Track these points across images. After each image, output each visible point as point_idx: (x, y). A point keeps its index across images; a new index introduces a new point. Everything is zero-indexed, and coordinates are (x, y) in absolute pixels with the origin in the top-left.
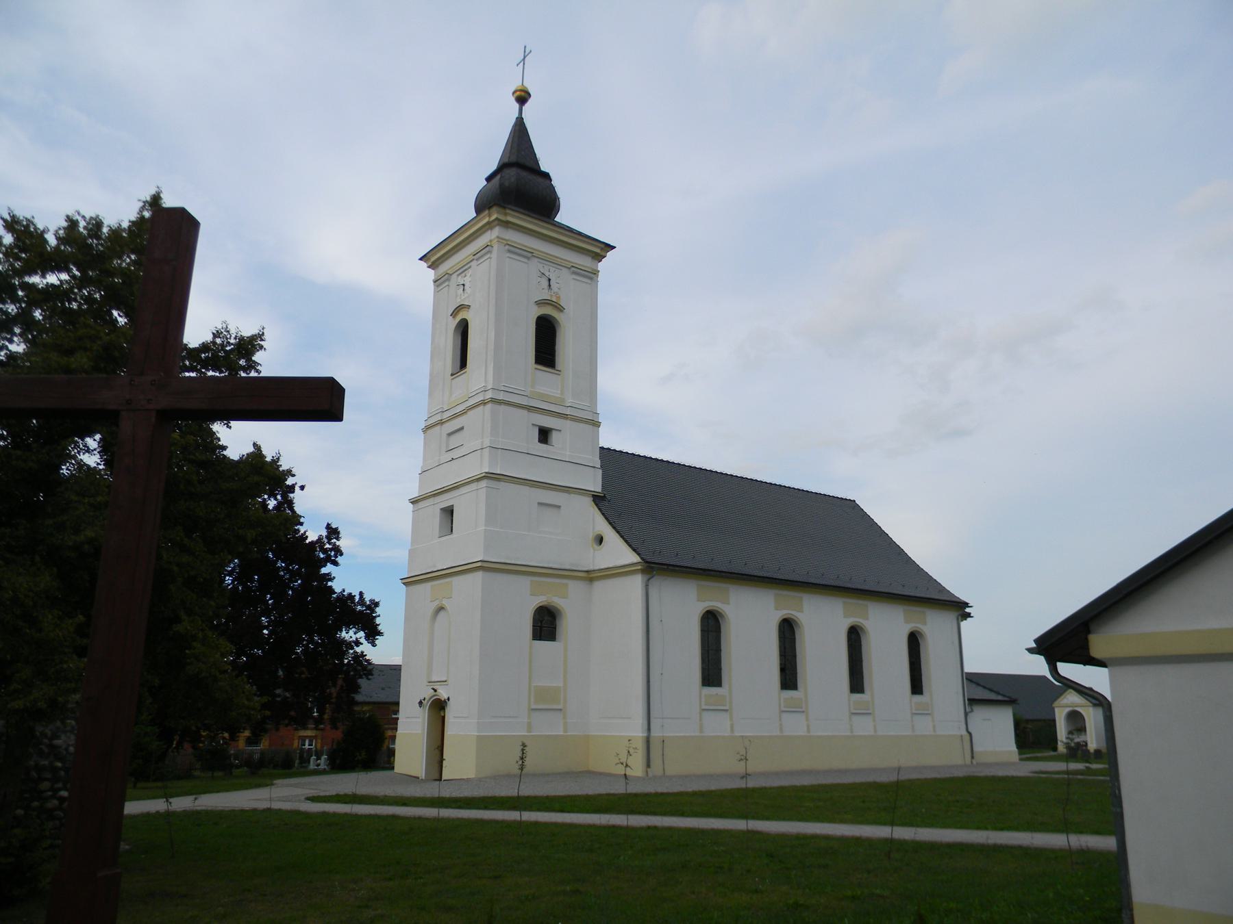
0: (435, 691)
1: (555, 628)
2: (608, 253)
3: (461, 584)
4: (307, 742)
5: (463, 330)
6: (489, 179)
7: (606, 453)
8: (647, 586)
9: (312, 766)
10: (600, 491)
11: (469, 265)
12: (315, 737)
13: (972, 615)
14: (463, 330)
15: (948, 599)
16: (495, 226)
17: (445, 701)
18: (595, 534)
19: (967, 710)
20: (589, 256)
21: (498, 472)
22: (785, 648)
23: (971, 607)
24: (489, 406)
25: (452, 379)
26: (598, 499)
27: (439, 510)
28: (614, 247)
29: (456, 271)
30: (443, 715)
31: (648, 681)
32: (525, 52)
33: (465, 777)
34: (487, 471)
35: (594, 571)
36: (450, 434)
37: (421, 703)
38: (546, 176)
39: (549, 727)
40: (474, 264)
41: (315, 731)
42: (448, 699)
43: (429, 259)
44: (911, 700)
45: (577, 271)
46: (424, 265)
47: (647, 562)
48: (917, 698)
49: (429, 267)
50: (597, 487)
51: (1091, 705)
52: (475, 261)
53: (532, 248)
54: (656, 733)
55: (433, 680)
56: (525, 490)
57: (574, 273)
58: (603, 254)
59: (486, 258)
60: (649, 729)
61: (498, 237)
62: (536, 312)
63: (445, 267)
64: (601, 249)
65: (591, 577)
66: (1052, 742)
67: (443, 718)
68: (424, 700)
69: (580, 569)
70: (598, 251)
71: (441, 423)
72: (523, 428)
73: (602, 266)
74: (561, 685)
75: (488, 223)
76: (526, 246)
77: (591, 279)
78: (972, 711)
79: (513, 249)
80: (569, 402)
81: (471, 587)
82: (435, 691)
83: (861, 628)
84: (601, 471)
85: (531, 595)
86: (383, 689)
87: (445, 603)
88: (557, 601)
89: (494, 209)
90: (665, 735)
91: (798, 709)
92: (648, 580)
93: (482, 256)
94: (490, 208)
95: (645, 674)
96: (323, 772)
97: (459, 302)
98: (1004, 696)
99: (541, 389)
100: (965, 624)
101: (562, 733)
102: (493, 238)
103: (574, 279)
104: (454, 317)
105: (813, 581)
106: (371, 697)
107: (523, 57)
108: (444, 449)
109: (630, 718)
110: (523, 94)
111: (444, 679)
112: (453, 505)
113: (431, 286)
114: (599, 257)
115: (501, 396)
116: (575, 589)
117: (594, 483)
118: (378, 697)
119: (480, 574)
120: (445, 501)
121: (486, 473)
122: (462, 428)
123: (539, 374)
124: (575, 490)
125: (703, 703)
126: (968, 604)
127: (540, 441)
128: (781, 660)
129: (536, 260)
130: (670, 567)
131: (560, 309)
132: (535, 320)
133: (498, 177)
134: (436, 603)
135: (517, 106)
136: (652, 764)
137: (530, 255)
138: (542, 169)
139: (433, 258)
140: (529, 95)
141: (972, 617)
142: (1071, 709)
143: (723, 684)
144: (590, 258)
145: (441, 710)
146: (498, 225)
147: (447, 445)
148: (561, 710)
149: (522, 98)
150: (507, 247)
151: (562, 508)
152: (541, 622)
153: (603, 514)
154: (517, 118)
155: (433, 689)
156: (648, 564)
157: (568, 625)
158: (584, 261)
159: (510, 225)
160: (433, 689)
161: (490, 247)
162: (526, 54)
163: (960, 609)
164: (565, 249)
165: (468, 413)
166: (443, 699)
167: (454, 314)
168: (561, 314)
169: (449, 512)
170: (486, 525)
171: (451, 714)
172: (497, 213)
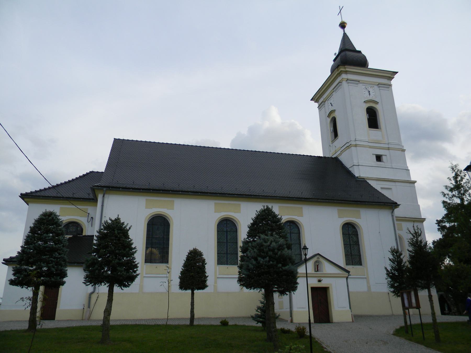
2: (395, 76)
6: (334, 60)
11: (332, 94)
20: (386, 79)
28: (398, 72)
38: (360, 52)
43: (315, 99)
46: (313, 102)
58: (392, 76)
64: (391, 75)
70: (390, 75)
73: (393, 82)
92: (392, 212)
113: (317, 109)
114: (391, 78)
131: (376, 103)
139: (315, 99)
143: (349, 271)
148: (366, 278)
149: (343, 25)
159: (348, 72)
167: (329, 116)
168: (377, 105)
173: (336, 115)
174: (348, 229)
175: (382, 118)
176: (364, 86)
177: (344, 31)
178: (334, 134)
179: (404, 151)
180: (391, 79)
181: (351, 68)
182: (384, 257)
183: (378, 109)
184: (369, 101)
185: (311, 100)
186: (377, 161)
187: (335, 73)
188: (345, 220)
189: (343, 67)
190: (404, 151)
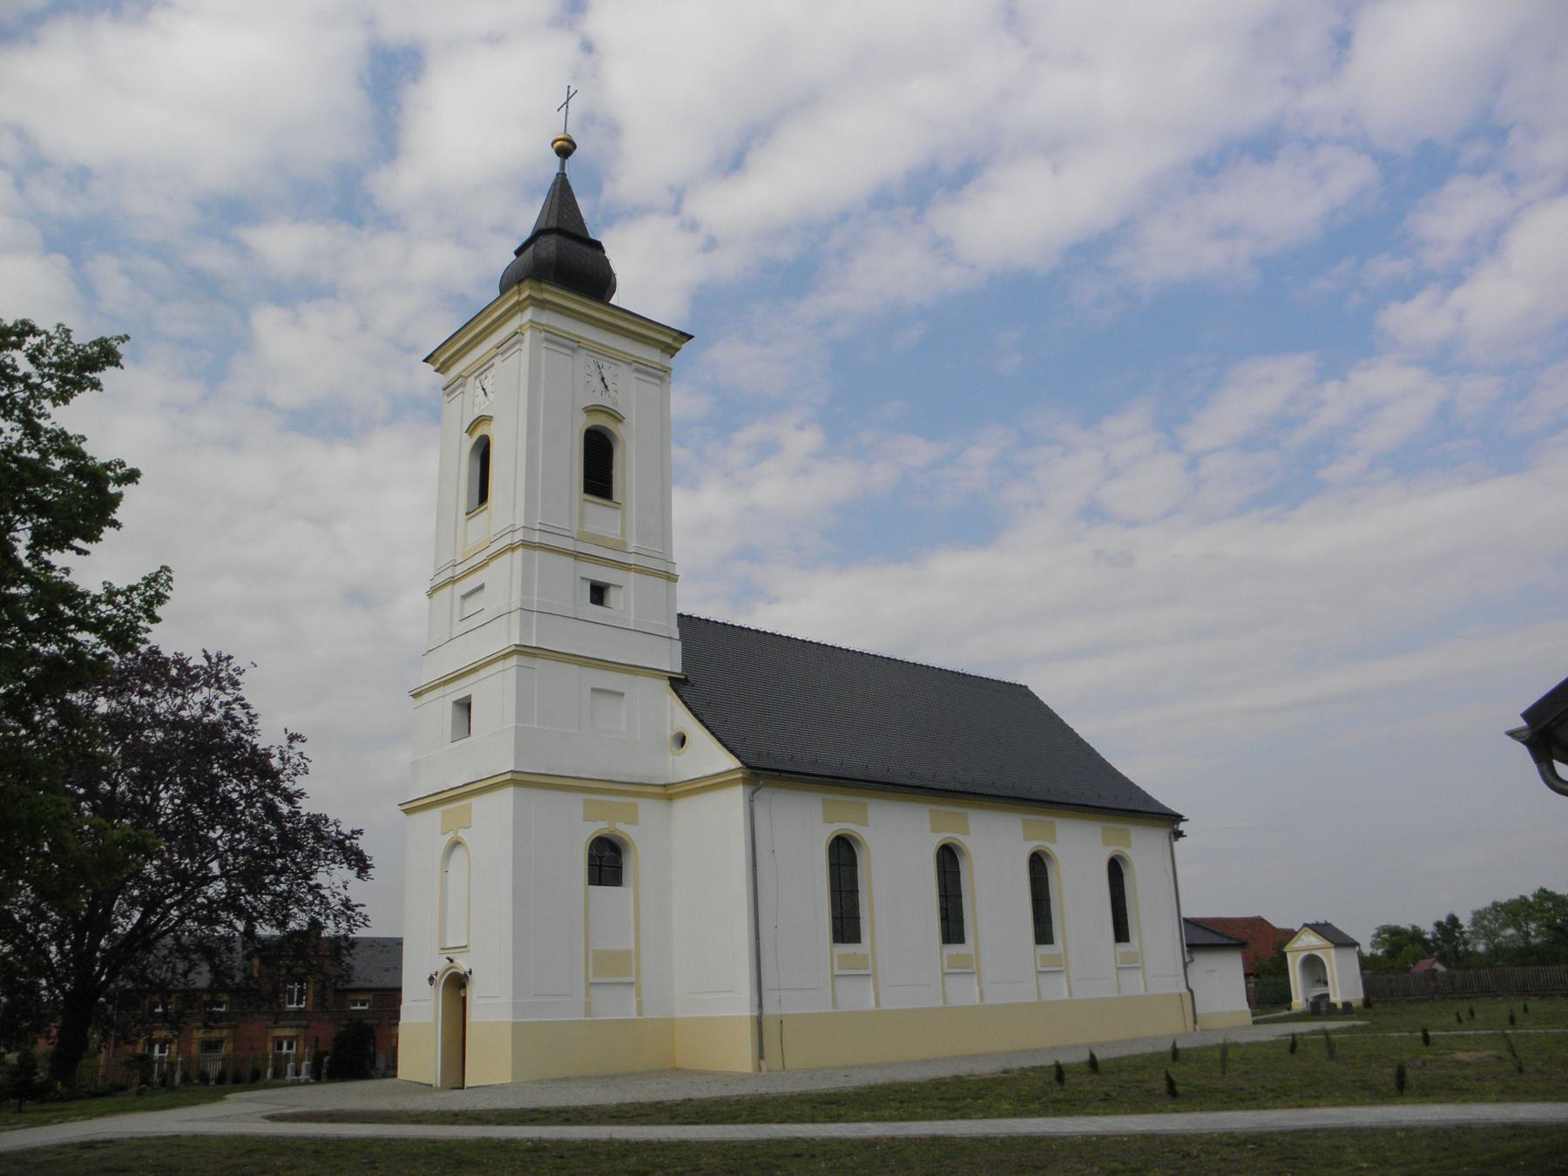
0: (451, 961)
1: (621, 868)
2: (683, 346)
3: (479, 805)
4: (157, 1048)
5: (483, 451)
6: (518, 253)
7: (686, 621)
8: (751, 801)
9: (290, 1076)
10: (680, 671)
11: (491, 363)
12: (296, 1037)
13: (1184, 834)
14: (483, 451)
15: (1156, 811)
16: (526, 308)
17: (465, 975)
18: (675, 732)
19: (1187, 959)
21: (534, 645)
22: (945, 886)
23: (1187, 820)
24: (519, 553)
25: (468, 519)
26: (677, 684)
27: (451, 704)
28: (690, 337)
29: (474, 372)
30: (463, 995)
31: (757, 938)
32: (568, 93)
33: (497, 1082)
34: (518, 643)
35: (673, 784)
36: (465, 597)
37: (431, 979)
39: (617, 1007)
40: (497, 360)
41: (296, 1030)
42: (470, 972)
43: (437, 359)
44: (1115, 950)
45: (642, 368)
47: (749, 767)
48: (1123, 947)
49: (437, 371)
50: (676, 667)
51: (1332, 945)
52: (499, 356)
53: (579, 337)
54: (770, 1009)
55: (448, 946)
56: (573, 670)
57: (637, 370)
59: (515, 349)
60: (760, 1006)
61: (531, 321)
62: (583, 423)
63: (454, 371)
65: (670, 792)
66: (1285, 998)
67: (464, 999)
68: (436, 974)
69: (656, 783)
70: (669, 340)
71: (453, 581)
72: (571, 581)
74: (632, 947)
75: (518, 303)
76: (569, 334)
77: (661, 379)
78: (1192, 960)
79: (553, 338)
80: (633, 544)
81: (499, 807)
82: (451, 961)
83: (1047, 855)
84: (680, 643)
85: (585, 820)
86: (387, 970)
87: (462, 834)
88: (623, 829)
89: (526, 283)
90: (783, 1013)
91: (966, 969)
92: (753, 793)
93: (508, 349)
94: (519, 282)
95: (753, 915)
96: (307, 1083)
97: (477, 413)
98: (1231, 939)
99: (591, 528)
100: (1179, 844)
101: (583, 1018)
102: (524, 321)
103: (637, 378)
104: (470, 435)
105: (978, 791)
106: (371, 981)
107: (566, 99)
108: (457, 618)
109: (732, 991)
110: (565, 143)
111: (464, 945)
112: (470, 697)
114: (671, 350)
115: (536, 538)
116: (647, 809)
117: (672, 661)
118: (381, 981)
119: (509, 792)
120: (458, 691)
121: (516, 645)
122: (481, 587)
123: (589, 506)
124: (642, 670)
125: (836, 966)
126: (1181, 816)
127: (593, 601)
128: (941, 902)
129: (584, 352)
130: (783, 774)
131: (618, 418)
132: (584, 432)
133: (531, 248)
134: (451, 835)
135: (558, 159)
136: (766, 1055)
137: (576, 345)
138: (591, 236)
140: (575, 146)
141: (1185, 836)
142: (1307, 953)
144: (659, 351)
145: (460, 988)
146: (532, 304)
147: (462, 608)
150: (543, 334)
151: (625, 696)
152: (601, 858)
153: (685, 703)
154: (558, 174)
155: (449, 959)
156: (752, 771)
157: (638, 864)
158: (653, 356)
159: (547, 305)
160: (449, 959)
161: (521, 336)
162: (570, 95)
163: (1170, 821)
164: (628, 340)
165: (490, 564)
166: (462, 973)
167: (471, 430)
169: (465, 706)
170: (517, 722)
171: (474, 994)
172: (530, 288)
173: (492, 431)
174: (839, 851)
175: (628, 468)
176: (592, 360)
177: (563, 166)
180: (672, 351)
181: (568, 297)
185: (426, 360)
187: (511, 297)
188: (944, 837)
189: (534, 284)
190: (671, 578)
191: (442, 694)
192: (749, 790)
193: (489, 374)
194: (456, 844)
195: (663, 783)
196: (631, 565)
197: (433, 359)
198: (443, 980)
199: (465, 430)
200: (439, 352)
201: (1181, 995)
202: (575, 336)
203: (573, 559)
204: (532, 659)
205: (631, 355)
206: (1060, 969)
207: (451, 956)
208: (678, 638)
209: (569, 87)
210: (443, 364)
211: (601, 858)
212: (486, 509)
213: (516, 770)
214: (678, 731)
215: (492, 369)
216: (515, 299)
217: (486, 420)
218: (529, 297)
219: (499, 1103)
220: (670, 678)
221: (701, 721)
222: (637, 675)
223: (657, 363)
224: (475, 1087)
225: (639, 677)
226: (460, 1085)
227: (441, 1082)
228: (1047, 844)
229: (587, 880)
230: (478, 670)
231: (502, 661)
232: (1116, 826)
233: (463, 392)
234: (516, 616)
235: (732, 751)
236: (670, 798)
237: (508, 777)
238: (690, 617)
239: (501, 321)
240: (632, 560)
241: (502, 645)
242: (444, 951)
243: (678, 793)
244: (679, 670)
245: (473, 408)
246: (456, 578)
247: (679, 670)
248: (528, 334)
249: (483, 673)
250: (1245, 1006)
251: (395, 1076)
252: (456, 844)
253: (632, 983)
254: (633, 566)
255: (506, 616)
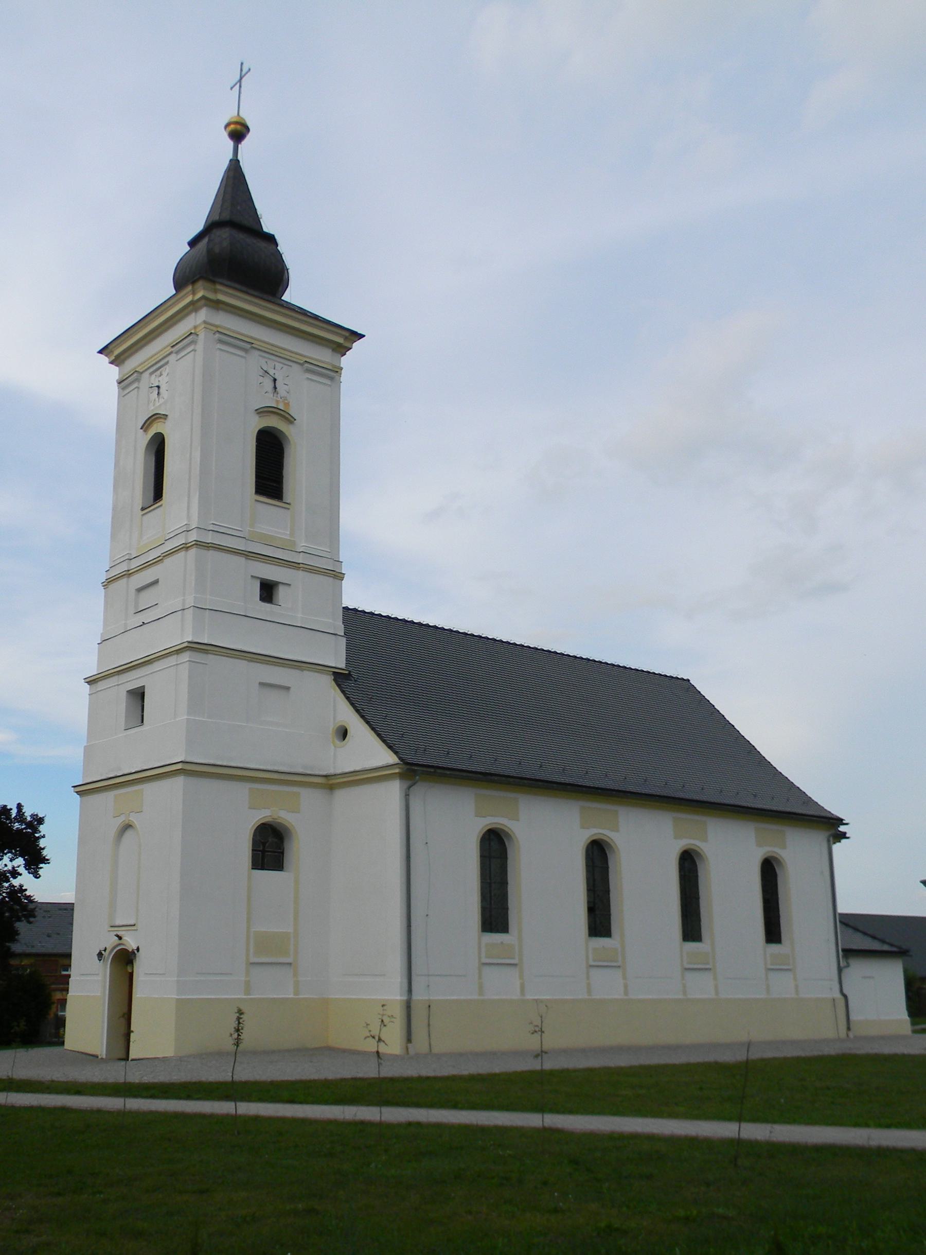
0: (120, 938)
1: (283, 853)
5: (158, 447)
6: (193, 243)
7: (352, 616)
11: (165, 360)
13: (847, 835)
14: (158, 447)
16: (200, 308)
17: (133, 952)
19: (842, 964)
20: (327, 346)
24: (193, 551)
26: (340, 678)
27: (125, 693)
28: (364, 336)
30: (130, 971)
31: (409, 926)
32: (241, 70)
34: (190, 640)
36: (140, 590)
37: (100, 955)
38: (271, 239)
40: (172, 358)
42: (138, 949)
43: (112, 352)
45: (310, 367)
46: (104, 359)
48: (774, 948)
49: (111, 363)
50: (339, 661)
54: (419, 995)
55: (117, 924)
56: (242, 665)
57: (308, 371)
58: (347, 344)
60: (410, 991)
61: (205, 322)
62: (256, 424)
68: (105, 950)
69: (317, 773)
70: (340, 340)
71: (128, 574)
73: (346, 361)
75: (192, 303)
78: (848, 966)
79: (226, 339)
82: (120, 938)
85: (250, 808)
87: (133, 818)
88: (285, 817)
89: (200, 284)
90: (431, 998)
92: (409, 787)
93: (183, 348)
94: (194, 283)
98: (892, 945)
99: (264, 528)
103: (308, 379)
104: (145, 431)
108: (132, 610)
109: (384, 975)
110: (239, 127)
111: (132, 922)
112: (144, 686)
114: (342, 350)
115: (209, 538)
116: (310, 799)
120: (133, 680)
121: (189, 642)
122: (156, 582)
123: (261, 507)
125: (483, 955)
126: (842, 820)
129: (257, 353)
133: (205, 240)
134: (121, 820)
135: (231, 144)
136: (414, 1037)
137: (249, 346)
149: (238, 133)
150: (217, 335)
153: (348, 698)
154: (231, 160)
155: (117, 936)
156: (408, 767)
158: (323, 355)
159: (221, 306)
160: (117, 936)
162: (244, 72)
165: (165, 561)
166: (130, 950)
167: (146, 426)
169: (139, 695)
172: (204, 289)
178: (154, 459)
179: (339, 576)
182: (428, 844)
183: (290, 438)
184: (266, 409)
185: (100, 352)
186: (260, 600)
188: (593, 833)
189: (208, 285)
191: (117, 684)
192: (406, 784)
193: (166, 370)
194: (128, 827)
195: (325, 773)
196: (299, 564)
197: (108, 351)
198: (113, 953)
199: (140, 427)
200: (114, 345)
201: (834, 1000)
202: (247, 336)
203: (244, 559)
204: (204, 656)
205: (305, 356)
206: (707, 966)
207: (120, 933)
208: (343, 634)
209: (242, 64)
210: (117, 357)
211: (264, 844)
212: (161, 506)
213: (188, 760)
214: (340, 724)
215: (167, 367)
216: (189, 299)
217: (161, 418)
218: (203, 297)
219: (162, 1077)
220: (334, 673)
221: (362, 717)
222: (302, 670)
223: (327, 363)
224: (139, 1060)
225: (305, 672)
226: (124, 1057)
227: (106, 1055)
228: (777, 850)
229: (251, 864)
230: (151, 663)
231: (176, 656)
232: (772, 827)
233: (138, 388)
234: (189, 614)
235: (390, 747)
236: (331, 788)
237: (179, 766)
238: (355, 610)
239: (174, 320)
240: (300, 559)
241: (176, 641)
242: (113, 929)
243: (339, 783)
244: (343, 665)
245: (148, 404)
246: (130, 572)
247: (343, 665)
248: (202, 336)
249: (157, 666)
250: (904, 1015)
251: (63, 1043)
252: (128, 827)
253: (290, 964)
254: (301, 565)
255: (180, 612)
